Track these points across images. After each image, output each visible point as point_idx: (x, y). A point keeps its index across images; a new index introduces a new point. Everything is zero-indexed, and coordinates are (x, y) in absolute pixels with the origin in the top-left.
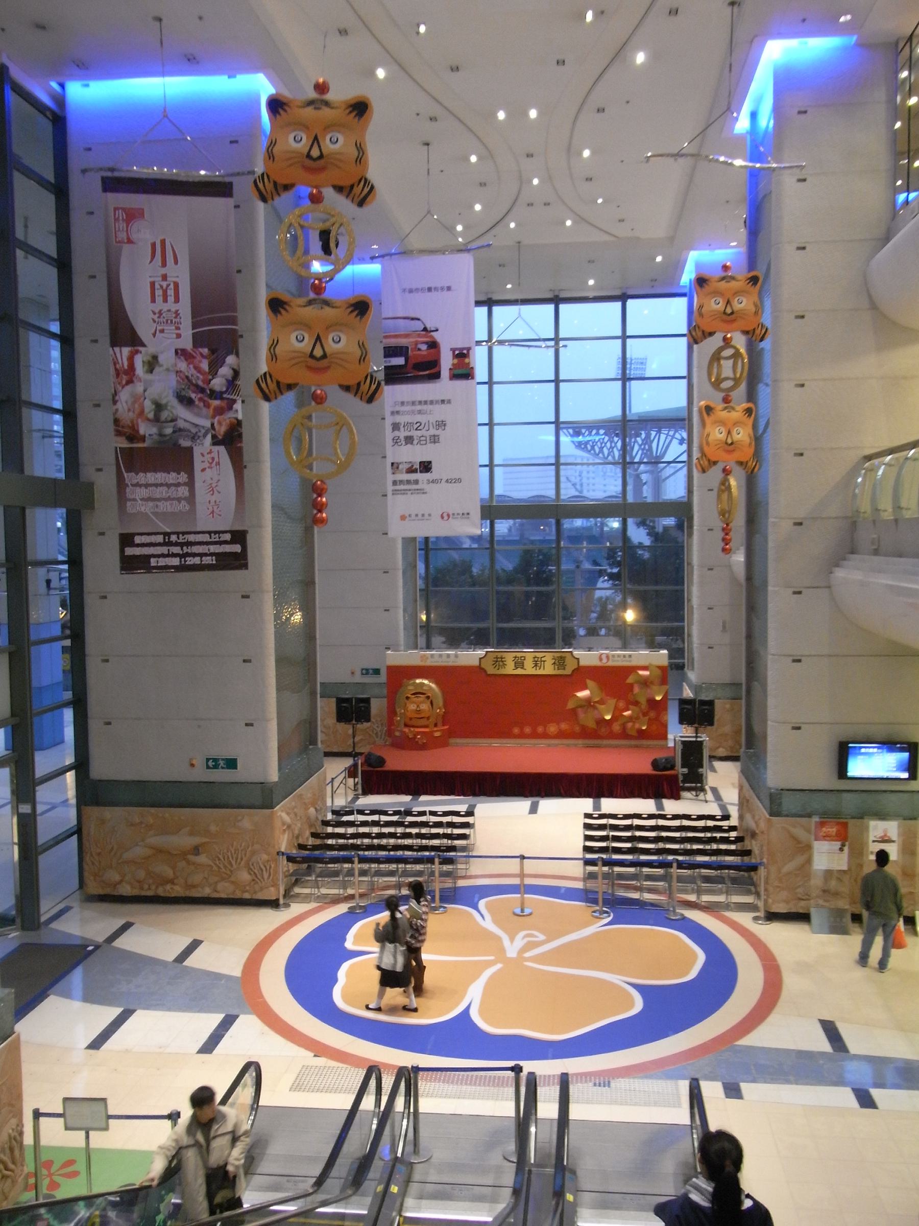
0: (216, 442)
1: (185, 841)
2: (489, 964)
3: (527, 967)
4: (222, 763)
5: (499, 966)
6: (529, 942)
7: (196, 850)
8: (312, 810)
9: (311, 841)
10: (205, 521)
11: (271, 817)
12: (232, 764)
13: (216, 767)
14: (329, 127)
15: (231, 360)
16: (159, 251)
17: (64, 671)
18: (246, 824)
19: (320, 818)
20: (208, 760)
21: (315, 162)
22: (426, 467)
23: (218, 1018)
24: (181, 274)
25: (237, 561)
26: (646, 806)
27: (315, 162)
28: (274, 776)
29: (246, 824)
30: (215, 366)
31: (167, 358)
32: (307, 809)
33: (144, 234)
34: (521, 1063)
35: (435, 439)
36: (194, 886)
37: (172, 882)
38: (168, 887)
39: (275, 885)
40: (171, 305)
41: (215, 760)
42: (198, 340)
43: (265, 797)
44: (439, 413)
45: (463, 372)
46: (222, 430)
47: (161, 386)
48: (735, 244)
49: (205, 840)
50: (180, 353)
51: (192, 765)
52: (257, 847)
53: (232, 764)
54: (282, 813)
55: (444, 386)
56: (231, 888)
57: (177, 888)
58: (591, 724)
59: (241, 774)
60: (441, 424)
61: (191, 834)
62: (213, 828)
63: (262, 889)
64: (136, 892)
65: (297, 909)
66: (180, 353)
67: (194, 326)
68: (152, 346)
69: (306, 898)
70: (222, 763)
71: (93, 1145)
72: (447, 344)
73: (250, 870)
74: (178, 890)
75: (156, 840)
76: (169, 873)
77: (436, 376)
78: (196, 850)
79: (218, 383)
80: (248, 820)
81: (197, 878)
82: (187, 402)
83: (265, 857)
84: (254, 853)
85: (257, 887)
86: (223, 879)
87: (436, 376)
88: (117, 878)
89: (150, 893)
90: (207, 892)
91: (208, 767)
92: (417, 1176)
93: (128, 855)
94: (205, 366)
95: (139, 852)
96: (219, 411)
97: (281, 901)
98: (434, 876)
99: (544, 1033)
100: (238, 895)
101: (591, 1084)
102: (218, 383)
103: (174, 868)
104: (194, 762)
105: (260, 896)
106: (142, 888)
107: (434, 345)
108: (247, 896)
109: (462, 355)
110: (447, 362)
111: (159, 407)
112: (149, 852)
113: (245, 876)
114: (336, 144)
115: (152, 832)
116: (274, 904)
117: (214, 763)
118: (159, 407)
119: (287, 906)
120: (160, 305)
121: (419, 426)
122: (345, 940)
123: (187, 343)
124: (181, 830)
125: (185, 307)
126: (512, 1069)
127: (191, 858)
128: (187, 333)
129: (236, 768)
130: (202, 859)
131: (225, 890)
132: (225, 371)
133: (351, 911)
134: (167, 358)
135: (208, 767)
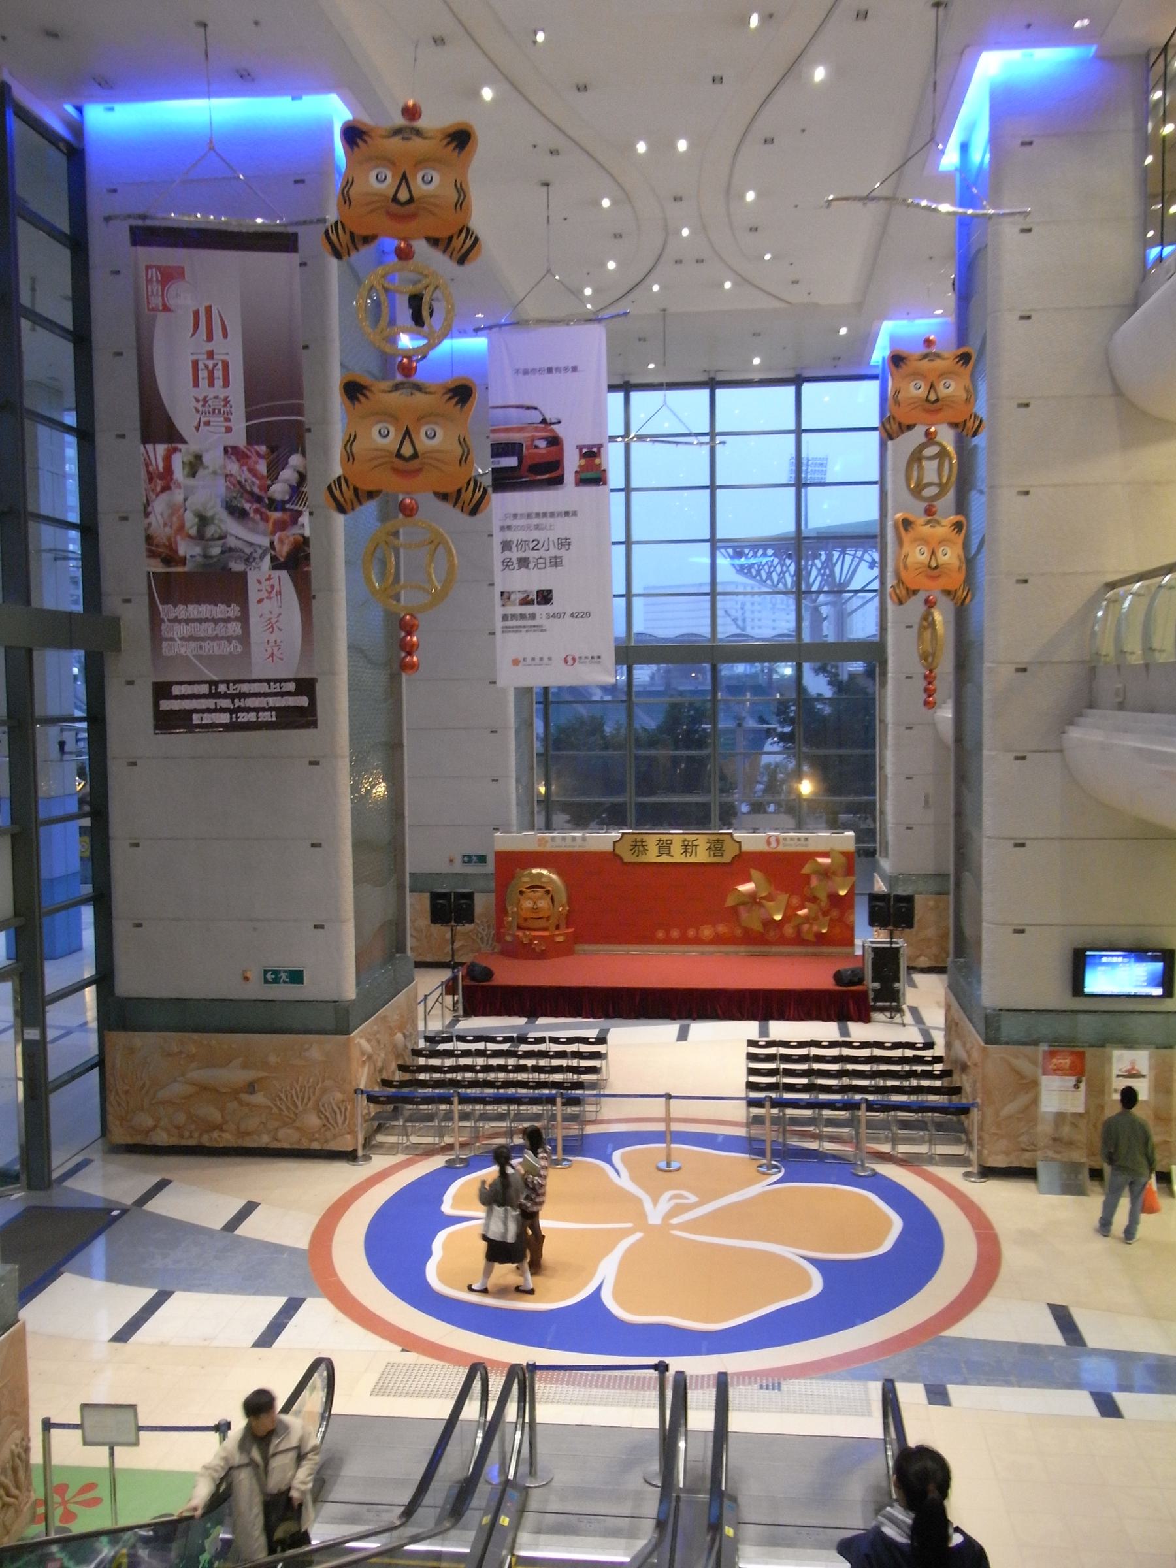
0: (276, 565)
1: (236, 1075)
2: (626, 1233)
3: (675, 1237)
4: (284, 976)
5: (639, 1235)
6: (677, 1205)
7: (251, 1088)
8: (399, 1036)
9: (398, 1076)
10: (262, 667)
11: (347, 1045)
12: (296, 977)
13: (276, 981)
14: (421, 162)
15: (295, 460)
16: (204, 321)
17: (82, 859)
18: (315, 1053)
19: (410, 1046)
20: (266, 972)
21: (403, 207)
22: (545, 597)
23: (279, 1302)
24: (232, 351)
25: (303, 718)
26: (827, 1030)
27: (403, 207)
28: (350, 992)
29: (315, 1053)
30: (275, 468)
31: (214, 458)
32: (393, 1034)
33: (184, 299)
34: (667, 1360)
35: (556, 562)
36: (248, 1134)
37: (220, 1128)
38: (215, 1134)
39: (352, 1132)
40: (218, 390)
41: (275, 972)
42: (254, 435)
43: (339, 1020)
44: (561, 528)
45: (592, 476)
46: (284, 550)
47: (206, 493)
48: (940, 312)
49: (262, 1074)
50: (231, 451)
51: (246, 979)
52: (329, 1083)
53: (296, 977)
54: (361, 1039)
55: (569, 494)
56: (296, 1136)
57: (227, 1136)
58: (757, 926)
59: (308, 990)
60: (565, 543)
61: (245, 1066)
62: (273, 1059)
63: (335, 1137)
64: (174, 1141)
65: (379, 1162)
66: (231, 451)
67: (249, 417)
68: (194, 443)
69: (392, 1149)
70: (284, 976)
71: (118, 1464)
72: (572, 440)
73: (319, 1113)
74: (228, 1139)
75: (199, 1075)
76: (217, 1116)
77: (558, 481)
78: (251, 1088)
79: (279, 490)
80: (317, 1048)
81: (252, 1123)
82: (240, 514)
83: (339, 1096)
84: (324, 1091)
85: (329, 1135)
86: (285, 1124)
87: (558, 481)
88: (150, 1122)
89: (192, 1142)
90: (265, 1140)
91: (266, 981)
92: (533, 1504)
93: (163, 1094)
94: (262, 467)
95: (178, 1089)
96: (281, 526)
97: (360, 1153)
98: (555, 1120)
99: (697, 1321)
100: (305, 1144)
101: (756, 1387)
102: (279, 490)
103: (222, 1110)
104: (248, 974)
105: (333, 1146)
106: (181, 1136)
107: (555, 441)
108: (316, 1146)
109: (591, 454)
110: (571, 463)
111: (203, 521)
112: (191, 1090)
113: (313, 1120)
114: (431, 184)
115: (194, 1065)
116: (350, 1156)
117: (273, 976)
118: (203, 521)
119: (367, 1158)
120: (204, 390)
121: (536, 545)
122: (441, 1202)
123: (239, 438)
124: (232, 1061)
125: (237, 392)
126: (655, 1367)
127: (245, 1097)
128: (240, 425)
129: (301, 982)
130: (259, 1098)
131: (288, 1138)
132: (288, 474)
133: (450, 1165)
134: (214, 458)
135: (266, 981)
